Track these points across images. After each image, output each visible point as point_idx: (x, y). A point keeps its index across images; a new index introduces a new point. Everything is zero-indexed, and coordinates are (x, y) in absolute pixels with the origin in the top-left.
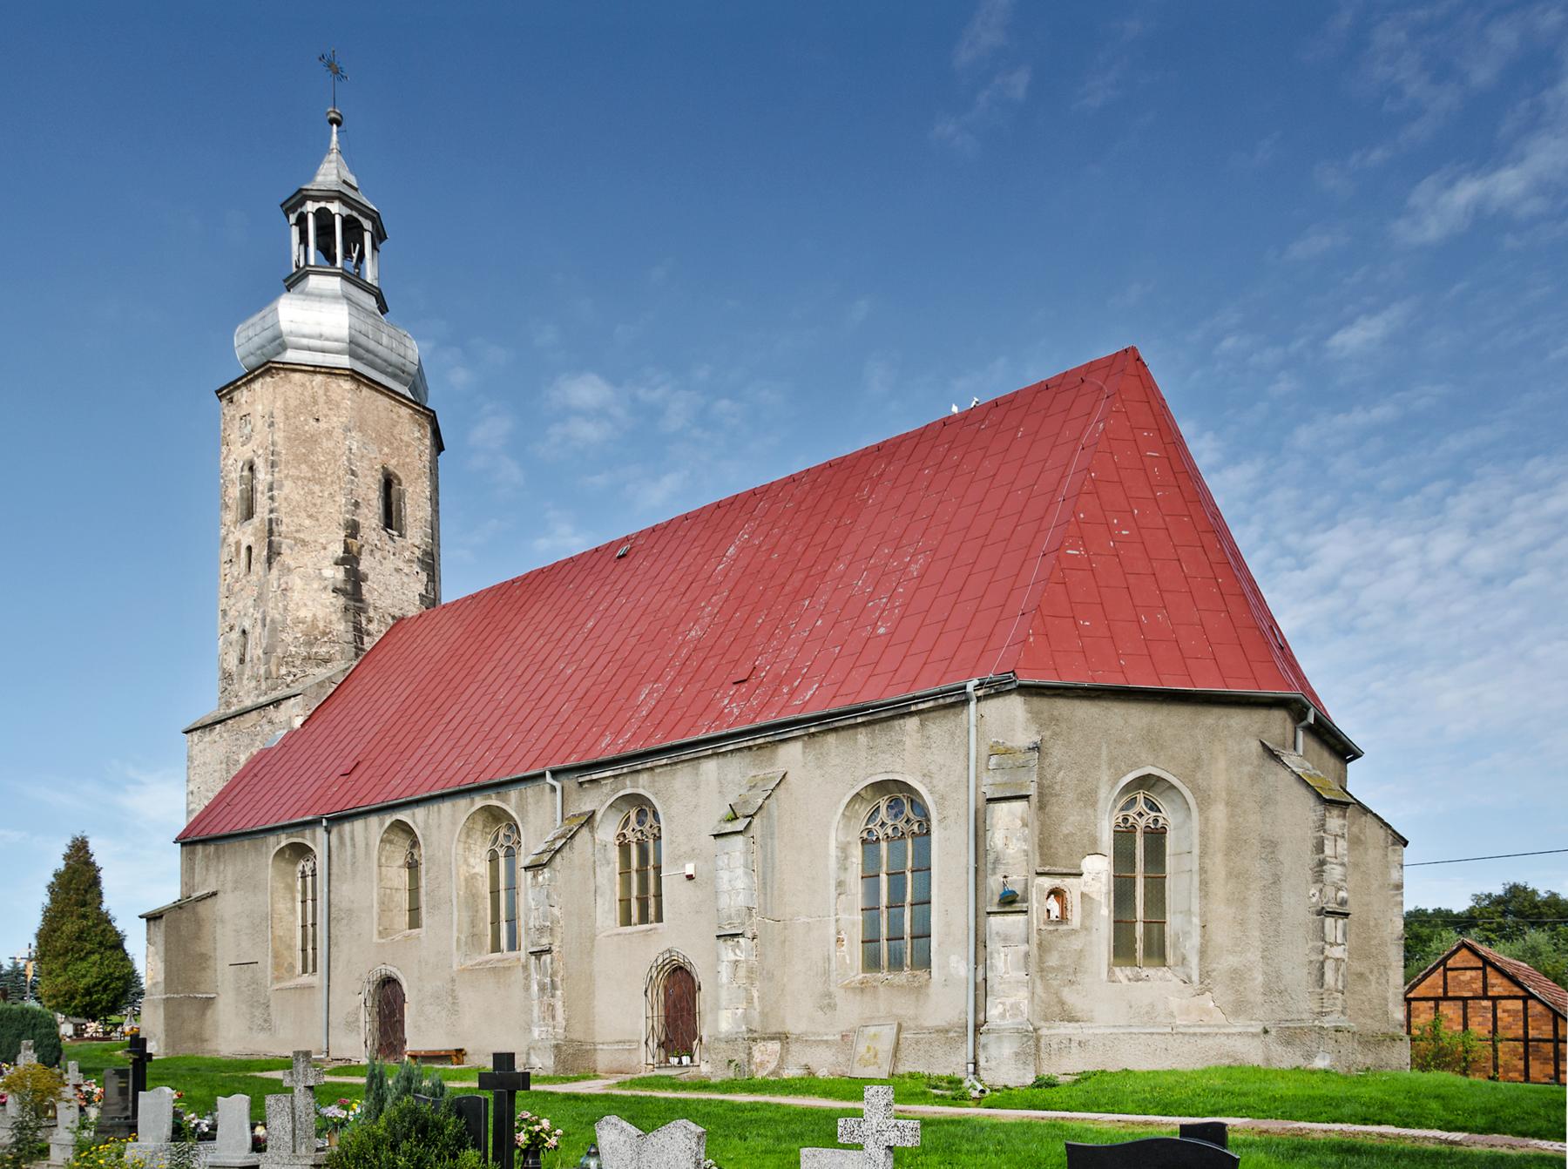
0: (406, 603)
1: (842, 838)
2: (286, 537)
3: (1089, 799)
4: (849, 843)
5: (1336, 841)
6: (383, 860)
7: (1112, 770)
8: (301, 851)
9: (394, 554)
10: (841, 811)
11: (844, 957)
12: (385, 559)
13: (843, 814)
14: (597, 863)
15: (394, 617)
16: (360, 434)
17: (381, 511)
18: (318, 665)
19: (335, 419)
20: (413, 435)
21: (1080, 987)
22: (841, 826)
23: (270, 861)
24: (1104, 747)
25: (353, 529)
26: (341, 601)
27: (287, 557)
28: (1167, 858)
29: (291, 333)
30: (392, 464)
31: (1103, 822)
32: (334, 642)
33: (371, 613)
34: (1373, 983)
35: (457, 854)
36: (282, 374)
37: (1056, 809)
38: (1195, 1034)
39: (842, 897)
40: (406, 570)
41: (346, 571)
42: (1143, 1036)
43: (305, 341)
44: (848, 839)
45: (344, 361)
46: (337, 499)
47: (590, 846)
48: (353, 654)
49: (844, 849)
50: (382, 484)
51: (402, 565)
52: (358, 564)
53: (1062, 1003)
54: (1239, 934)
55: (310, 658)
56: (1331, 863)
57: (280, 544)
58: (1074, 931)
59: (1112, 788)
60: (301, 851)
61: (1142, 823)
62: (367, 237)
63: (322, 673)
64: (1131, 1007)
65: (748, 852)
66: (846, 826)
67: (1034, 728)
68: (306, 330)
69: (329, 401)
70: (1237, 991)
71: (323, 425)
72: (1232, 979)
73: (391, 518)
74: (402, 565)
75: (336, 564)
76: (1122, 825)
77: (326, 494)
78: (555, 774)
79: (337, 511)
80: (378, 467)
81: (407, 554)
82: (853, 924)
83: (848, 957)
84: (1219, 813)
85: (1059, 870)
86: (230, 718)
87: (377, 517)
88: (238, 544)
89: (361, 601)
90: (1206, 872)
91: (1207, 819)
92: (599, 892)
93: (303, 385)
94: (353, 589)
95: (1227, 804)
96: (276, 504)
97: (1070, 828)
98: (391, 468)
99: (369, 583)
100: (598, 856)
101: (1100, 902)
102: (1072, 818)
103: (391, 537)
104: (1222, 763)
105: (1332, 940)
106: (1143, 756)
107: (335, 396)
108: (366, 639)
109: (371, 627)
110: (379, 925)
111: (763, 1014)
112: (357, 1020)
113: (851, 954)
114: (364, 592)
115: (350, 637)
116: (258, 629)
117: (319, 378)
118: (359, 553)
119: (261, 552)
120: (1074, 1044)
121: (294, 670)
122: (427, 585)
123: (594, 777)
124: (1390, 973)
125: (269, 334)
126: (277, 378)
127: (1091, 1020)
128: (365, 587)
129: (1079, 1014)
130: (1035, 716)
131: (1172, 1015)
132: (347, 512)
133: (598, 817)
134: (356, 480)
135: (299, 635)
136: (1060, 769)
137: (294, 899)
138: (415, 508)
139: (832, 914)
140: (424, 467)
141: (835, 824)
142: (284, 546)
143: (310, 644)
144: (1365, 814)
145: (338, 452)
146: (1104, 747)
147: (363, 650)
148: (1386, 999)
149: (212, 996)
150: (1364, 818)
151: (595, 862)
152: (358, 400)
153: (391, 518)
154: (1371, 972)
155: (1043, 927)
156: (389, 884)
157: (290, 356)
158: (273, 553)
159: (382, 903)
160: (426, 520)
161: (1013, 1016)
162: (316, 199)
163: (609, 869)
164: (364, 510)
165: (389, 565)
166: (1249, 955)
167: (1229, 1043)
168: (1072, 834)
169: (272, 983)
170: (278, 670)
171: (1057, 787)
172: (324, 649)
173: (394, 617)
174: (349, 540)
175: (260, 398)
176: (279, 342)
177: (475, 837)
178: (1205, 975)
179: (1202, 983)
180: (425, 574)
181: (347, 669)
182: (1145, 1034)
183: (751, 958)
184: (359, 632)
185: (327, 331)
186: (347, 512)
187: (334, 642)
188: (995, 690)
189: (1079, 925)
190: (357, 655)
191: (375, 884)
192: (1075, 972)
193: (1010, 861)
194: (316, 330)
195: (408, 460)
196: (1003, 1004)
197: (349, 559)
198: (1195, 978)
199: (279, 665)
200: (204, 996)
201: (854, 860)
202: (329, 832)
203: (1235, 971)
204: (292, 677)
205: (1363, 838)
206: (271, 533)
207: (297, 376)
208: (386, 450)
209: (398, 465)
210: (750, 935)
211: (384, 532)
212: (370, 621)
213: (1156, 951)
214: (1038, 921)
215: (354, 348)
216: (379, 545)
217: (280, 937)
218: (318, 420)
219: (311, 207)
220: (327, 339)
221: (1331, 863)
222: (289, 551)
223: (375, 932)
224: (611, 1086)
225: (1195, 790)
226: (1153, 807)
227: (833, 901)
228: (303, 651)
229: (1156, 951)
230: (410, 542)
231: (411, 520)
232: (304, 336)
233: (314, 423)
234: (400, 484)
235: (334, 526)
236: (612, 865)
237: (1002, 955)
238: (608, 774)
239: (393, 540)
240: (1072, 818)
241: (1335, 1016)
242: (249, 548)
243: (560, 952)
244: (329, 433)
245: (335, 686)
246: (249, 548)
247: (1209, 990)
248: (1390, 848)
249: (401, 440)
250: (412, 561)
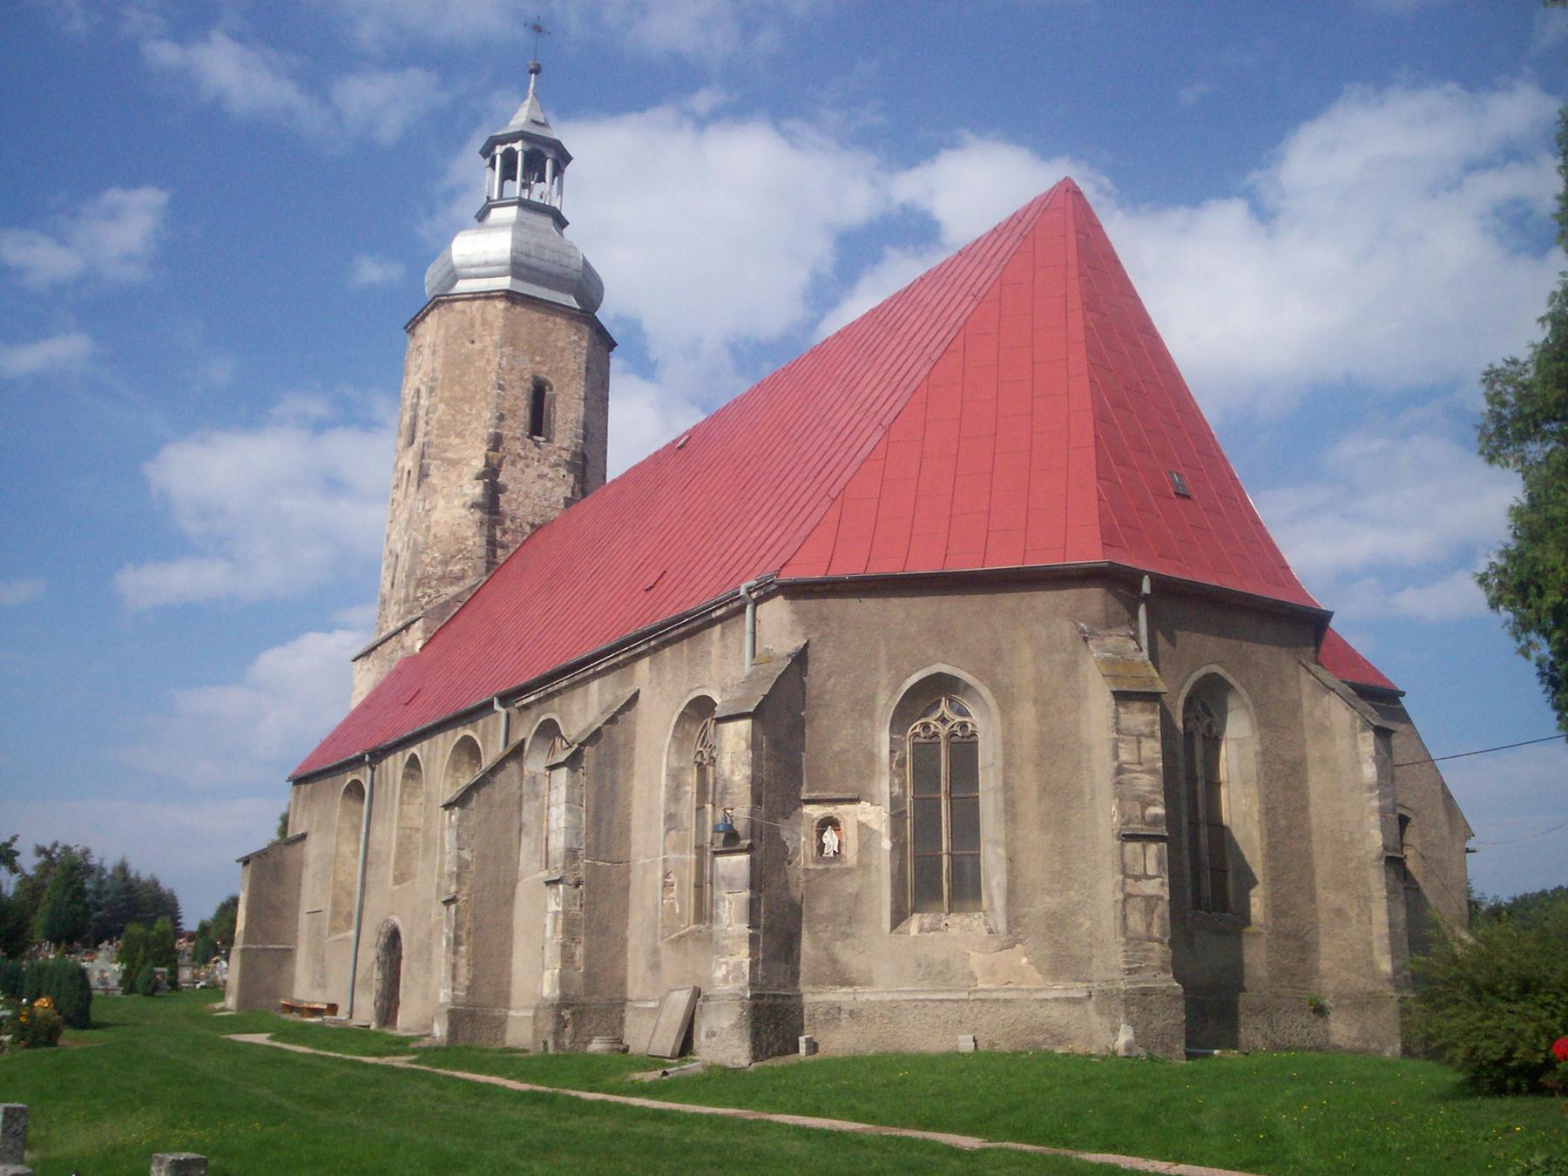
0: (548, 509)
1: (675, 764)
2: (434, 459)
3: (865, 709)
4: (683, 769)
5: (1139, 742)
6: (405, 798)
7: (893, 672)
8: (355, 790)
9: (539, 461)
10: (671, 732)
11: (672, 905)
12: (528, 467)
13: (673, 736)
14: (525, 798)
15: (532, 526)
16: (511, 348)
17: (527, 420)
18: (451, 584)
19: (488, 339)
20: (569, 342)
21: (853, 941)
22: (672, 750)
23: (340, 799)
24: (882, 644)
25: (496, 442)
26: (478, 514)
27: (435, 478)
28: (980, 772)
29: (462, 266)
30: (543, 372)
31: (882, 735)
32: (468, 558)
33: (508, 523)
34: (1354, 922)
35: (444, 789)
36: (446, 305)
37: (825, 722)
38: (997, 1001)
39: (673, 833)
40: (551, 475)
41: (485, 484)
42: (930, 1005)
43: (473, 271)
44: (682, 764)
45: (505, 283)
46: (483, 414)
47: (516, 779)
48: (484, 569)
49: (676, 778)
50: (531, 393)
51: (545, 470)
52: (498, 476)
53: (834, 961)
54: (1057, 867)
55: (445, 577)
56: (1131, 771)
57: (429, 465)
58: (849, 871)
59: (894, 693)
60: (355, 790)
61: (943, 731)
62: (549, 165)
63: (452, 590)
64: (919, 965)
65: (570, 787)
66: (679, 751)
67: (800, 630)
68: (475, 260)
69: (484, 322)
70: (1056, 942)
71: (478, 345)
72: (1049, 926)
73: (538, 424)
74: (545, 470)
75: (477, 479)
76: (922, 735)
77: (474, 412)
78: (505, 699)
79: (482, 422)
80: (527, 376)
81: (553, 459)
82: (684, 864)
83: (677, 906)
84: (1026, 715)
85: (827, 795)
86: (379, 645)
87: (522, 426)
88: (403, 468)
89: (497, 513)
90: (1012, 788)
91: (1011, 724)
92: (524, 832)
93: (464, 312)
94: (491, 504)
95: (1036, 702)
96: (430, 428)
97: (842, 744)
98: (542, 376)
99: (507, 494)
100: (525, 789)
101: (880, 833)
102: (844, 732)
103: (537, 444)
104: (1027, 653)
105: (1139, 870)
106: (931, 652)
107: (490, 318)
108: (499, 552)
109: (508, 538)
110: (395, 869)
111: (589, 975)
112: (371, 978)
113: (682, 903)
114: (501, 504)
115: (482, 552)
116: (405, 552)
117: (477, 303)
118: (500, 465)
119: (414, 475)
120: (844, 1015)
121: (429, 591)
122: (573, 488)
123: (525, 701)
124: (1373, 906)
125: (444, 271)
126: (442, 309)
127: (869, 983)
128: (502, 498)
129: (854, 976)
130: (802, 618)
131: (972, 976)
132: (491, 426)
133: (527, 746)
134: (503, 393)
135: (437, 555)
136: (830, 676)
137: (358, 840)
138: (567, 413)
139: (661, 853)
140: (579, 368)
141: (666, 748)
142: (432, 468)
143: (446, 563)
144: (1328, 693)
145: (489, 369)
146: (882, 644)
147: (497, 563)
148: (1370, 944)
149: (291, 947)
150: (1327, 698)
151: (521, 796)
152: (512, 316)
153: (538, 424)
154: (1351, 907)
155: (811, 866)
156: (409, 824)
157: (463, 286)
158: (423, 474)
159: (400, 845)
160: (577, 422)
161: (736, 979)
162: (503, 143)
163: (537, 804)
164: (509, 422)
165: (531, 473)
166: (1072, 893)
167: (1043, 1013)
168: (843, 752)
169: (329, 934)
170: (415, 592)
171: (827, 697)
172: (458, 567)
173: (532, 526)
174: (491, 454)
175: (430, 329)
176: (454, 276)
177: (463, 770)
178: (1013, 921)
179: (1010, 932)
180: (572, 476)
181: (475, 585)
182: (934, 1001)
183: (573, 908)
184: (492, 544)
185: (492, 257)
186: (491, 426)
187: (468, 558)
188: (766, 592)
189: (855, 862)
190: (488, 570)
191: (395, 824)
192: (850, 921)
193: (736, 790)
194: (483, 258)
195: (561, 365)
196: (726, 963)
197: (490, 475)
198: (1002, 926)
199: (417, 586)
200: (282, 947)
201: (688, 788)
202: (373, 769)
203: (1052, 915)
204: (427, 599)
205: (1328, 724)
206: (423, 456)
207: (458, 305)
208: (538, 359)
209: (550, 370)
210: (571, 881)
211: (529, 441)
212: (505, 532)
213: (967, 891)
214: (806, 859)
215: (518, 268)
216: (522, 454)
217: (342, 882)
218: (473, 342)
219: (499, 150)
220: (491, 265)
221: (1131, 771)
222: (436, 472)
223: (391, 878)
224: (410, 1062)
225: (995, 688)
226: (962, 712)
227: (662, 838)
228: (439, 570)
229: (967, 891)
230: (558, 445)
231: (560, 423)
232: (472, 266)
233: (470, 345)
234: (551, 389)
235: (478, 444)
236: (541, 799)
237: (727, 903)
238: (532, 698)
239: (539, 447)
240: (844, 732)
241: (1148, 974)
242: (409, 472)
243: (467, 901)
244: (482, 351)
245: (460, 605)
246: (409, 472)
247: (1020, 941)
248: (1359, 736)
249: (556, 347)
250: (559, 465)
